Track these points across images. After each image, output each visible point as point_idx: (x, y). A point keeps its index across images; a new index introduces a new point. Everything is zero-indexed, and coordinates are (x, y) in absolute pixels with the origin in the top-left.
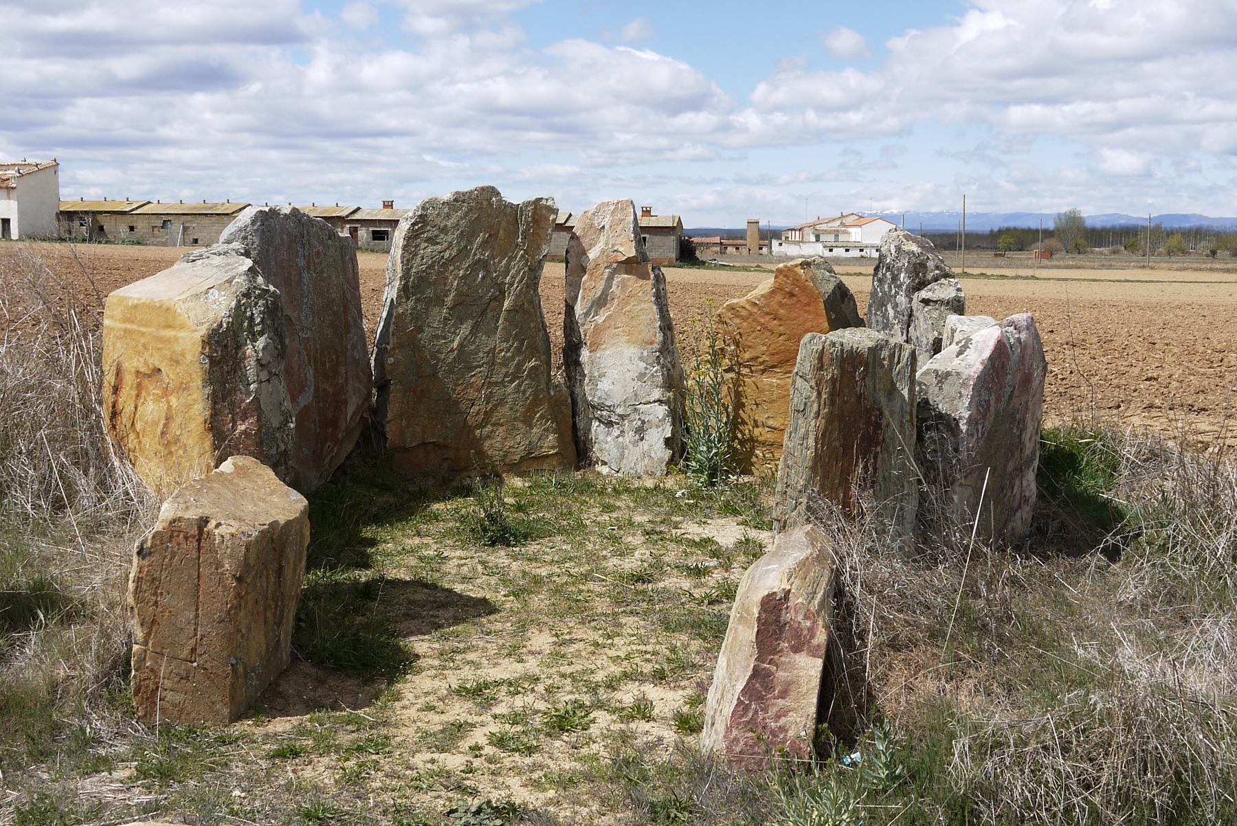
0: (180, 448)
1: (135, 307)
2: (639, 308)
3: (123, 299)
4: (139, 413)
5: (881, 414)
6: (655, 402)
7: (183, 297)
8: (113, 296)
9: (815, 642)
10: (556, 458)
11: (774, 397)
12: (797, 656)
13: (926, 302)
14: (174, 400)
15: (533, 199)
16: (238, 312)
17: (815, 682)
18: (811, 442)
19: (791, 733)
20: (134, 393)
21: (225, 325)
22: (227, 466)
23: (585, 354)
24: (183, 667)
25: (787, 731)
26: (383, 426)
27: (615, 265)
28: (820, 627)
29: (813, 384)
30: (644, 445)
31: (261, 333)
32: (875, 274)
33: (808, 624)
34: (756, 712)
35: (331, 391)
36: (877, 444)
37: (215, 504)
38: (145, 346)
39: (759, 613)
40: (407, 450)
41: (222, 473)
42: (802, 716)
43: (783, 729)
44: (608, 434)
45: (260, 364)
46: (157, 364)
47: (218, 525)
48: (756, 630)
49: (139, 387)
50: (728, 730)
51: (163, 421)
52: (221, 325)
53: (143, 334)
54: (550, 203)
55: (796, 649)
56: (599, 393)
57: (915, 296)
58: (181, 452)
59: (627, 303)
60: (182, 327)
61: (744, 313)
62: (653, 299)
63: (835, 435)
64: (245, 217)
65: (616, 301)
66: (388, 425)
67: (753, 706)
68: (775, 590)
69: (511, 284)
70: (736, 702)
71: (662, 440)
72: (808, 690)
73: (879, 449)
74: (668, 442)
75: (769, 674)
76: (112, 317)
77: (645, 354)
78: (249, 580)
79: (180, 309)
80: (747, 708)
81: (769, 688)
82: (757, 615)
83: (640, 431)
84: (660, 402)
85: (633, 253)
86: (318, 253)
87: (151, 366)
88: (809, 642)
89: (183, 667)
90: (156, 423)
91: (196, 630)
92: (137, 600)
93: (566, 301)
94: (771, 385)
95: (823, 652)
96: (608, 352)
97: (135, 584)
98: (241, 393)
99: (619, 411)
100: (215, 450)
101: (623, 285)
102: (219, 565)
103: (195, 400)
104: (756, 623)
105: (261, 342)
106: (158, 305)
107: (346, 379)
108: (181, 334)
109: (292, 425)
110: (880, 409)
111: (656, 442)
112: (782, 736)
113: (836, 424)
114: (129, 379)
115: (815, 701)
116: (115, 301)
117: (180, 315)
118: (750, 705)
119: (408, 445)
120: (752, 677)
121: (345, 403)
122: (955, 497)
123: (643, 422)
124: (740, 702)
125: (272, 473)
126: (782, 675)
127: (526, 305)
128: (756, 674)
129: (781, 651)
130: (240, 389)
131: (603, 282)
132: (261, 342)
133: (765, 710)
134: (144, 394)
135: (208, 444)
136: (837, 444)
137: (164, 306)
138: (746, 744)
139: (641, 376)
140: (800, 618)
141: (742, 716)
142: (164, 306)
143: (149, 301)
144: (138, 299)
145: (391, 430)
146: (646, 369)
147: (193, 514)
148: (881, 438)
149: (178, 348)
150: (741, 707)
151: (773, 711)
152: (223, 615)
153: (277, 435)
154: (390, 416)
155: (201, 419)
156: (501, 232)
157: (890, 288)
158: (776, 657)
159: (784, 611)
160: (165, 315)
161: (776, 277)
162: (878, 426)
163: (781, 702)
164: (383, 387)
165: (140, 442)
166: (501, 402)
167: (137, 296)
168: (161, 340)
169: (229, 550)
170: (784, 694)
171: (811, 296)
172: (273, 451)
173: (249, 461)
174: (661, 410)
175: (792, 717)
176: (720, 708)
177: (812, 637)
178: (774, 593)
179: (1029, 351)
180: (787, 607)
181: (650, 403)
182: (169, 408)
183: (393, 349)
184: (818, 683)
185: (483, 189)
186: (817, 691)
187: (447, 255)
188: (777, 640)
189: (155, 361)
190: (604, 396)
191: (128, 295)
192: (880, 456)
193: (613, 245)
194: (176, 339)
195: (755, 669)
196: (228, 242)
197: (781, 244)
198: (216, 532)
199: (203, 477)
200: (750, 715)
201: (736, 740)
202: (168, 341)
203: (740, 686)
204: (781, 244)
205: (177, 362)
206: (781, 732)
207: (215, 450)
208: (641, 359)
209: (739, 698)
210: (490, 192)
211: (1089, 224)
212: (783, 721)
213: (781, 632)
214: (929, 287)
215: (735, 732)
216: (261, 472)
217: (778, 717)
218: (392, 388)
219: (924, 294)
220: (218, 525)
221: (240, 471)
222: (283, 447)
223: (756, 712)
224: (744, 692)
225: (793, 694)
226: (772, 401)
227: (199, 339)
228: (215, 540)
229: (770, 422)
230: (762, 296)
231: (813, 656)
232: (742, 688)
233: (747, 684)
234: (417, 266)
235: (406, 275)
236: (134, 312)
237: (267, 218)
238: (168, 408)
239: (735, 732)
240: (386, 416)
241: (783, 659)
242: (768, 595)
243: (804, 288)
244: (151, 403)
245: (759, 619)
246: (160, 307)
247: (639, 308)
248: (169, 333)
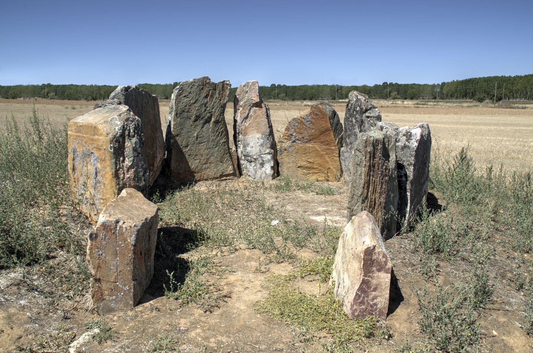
2: (261, 120)
3: (76, 123)
6: (267, 153)
7: (101, 122)
9: (387, 267)
11: (310, 151)
12: (380, 274)
13: (368, 117)
15: (222, 81)
16: (124, 129)
17: (388, 284)
18: (363, 177)
19: (379, 306)
21: (119, 134)
22: (124, 193)
23: (241, 137)
24: (112, 285)
25: (377, 305)
27: (252, 105)
28: (389, 261)
29: (363, 153)
30: (263, 169)
31: (134, 136)
32: (347, 107)
33: (384, 260)
34: (364, 298)
35: (151, 153)
37: (121, 213)
39: (364, 256)
41: (122, 197)
42: (383, 299)
43: (375, 304)
44: (251, 165)
45: (135, 150)
47: (124, 223)
48: (362, 263)
50: (352, 306)
52: (117, 134)
53: (84, 137)
54: (228, 82)
55: (379, 270)
57: (364, 115)
59: (256, 118)
60: (101, 135)
61: (299, 121)
62: (266, 117)
64: (119, 89)
65: (252, 118)
67: (363, 295)
68: (370, 246)
69: (215, 112)
71: (270, 167)
72: (385, 287)
74: (272, 168)
75: (369, 281)
76: (71, 131)
79: (100, 127)
80: (360, 296)
81: (369, 287)
82: (363, 257)
83: (262, 165)
84: (269, 153)
85: (258, 100)
86: (145, 103)
88: (385, 267)
89: (112, 285)
91: (117, 268)
92: (91, 258)
93: (463, 148)
94: (309, 147)
95: (390, 271)
96: (250, 136)
97: (90, 251)
99: (255, 157)
100: (117, 185)
101: (255, 112)
102: (125, 240)
103: (107, 165)
104: (362, 260)
105: (134, 140)
106: (90, 125)
107: (157, 149)
108: (101, 138)
111: (268, 169)
112: (375, 307)
115: (388, 292)
116: (72, 124)
117: (100, 130)
120: (361, 283)
121: (156, 157)
124: (357, 294)
125: (142, 195)
126: (374, 282)
128: (364, 282)
129: (373, 271)
131: (248, 111)
132: (134, 140)
133: (368, 297)
135: (114, 184)
137: (93, 126)
138: (360, 312)
139: (262, 145)
140: (381, 257)
141: (357, 300)
142: (93, 126)
143: (86, 124)
144: (82, 123)
147: (113, 219)
149: (100, 144)
150: (357, 296)
151: (371, 297)
152: (128, 261)
155: (110, 173)
158: (371, 274)
159: (373, 255)
160: (93, 129)
161: (311, 108)
163: (374, 293)
166: (212, 155)
167: (81, 122)
168: (92, 140)
169: (129, 234)
170: (375, 290)
171: (324, 114)
173: (132, 190)
174: (269, 157)
175: (379, 299)
176: (347, 296)
177: (386, 265)
178: (370, 247)
180: (375, 253)
181: (265, 154)
184: (389, 285)
185: (204, 78)
186: (389, 288)
187: (191, 102)
188: (371, 267)
190: (249, 152)
191: (78, 121)
193: (251, 97)
194: (99, 140)
195: (363, 280)
196: (113, 99)
198: (124, 226)
199: (115, 199)
200: (361, 299)
201: (356, 310)
202: (96, 140)
203: (357, 287)
205: (100, 149)
206: (375, 306)
207: (117, 185)
208: (262, 138)
209: (356, 293)
211: (88, 86)
212: (375, 301)
213: (373, 264)
214: (368, 112)
215: (355, 307)
216: (138, 195)
217: (373, 299)
218: (173, 151)
219: (367, 114)
220: (124, 223)
221: (130, 195)
223: (364, 298)
224: (358, 290)
225: (379, 290)
226: (310, 153)
227: (109, 140)
228: (123, 229)
229: (309, 160)
231: (387, 273)
232: (357, 288)
233: (360, 286)
234: (181, 106)
235: (177, 108)
236: (80, 128)
237: (127, 89)
239: (355, 307)
241: (374, 275)
242: (368, 248)
243: (321, 112)
245: (364, 259)
246: (91, 127)
247: (261, 120)
248: (96, 137)
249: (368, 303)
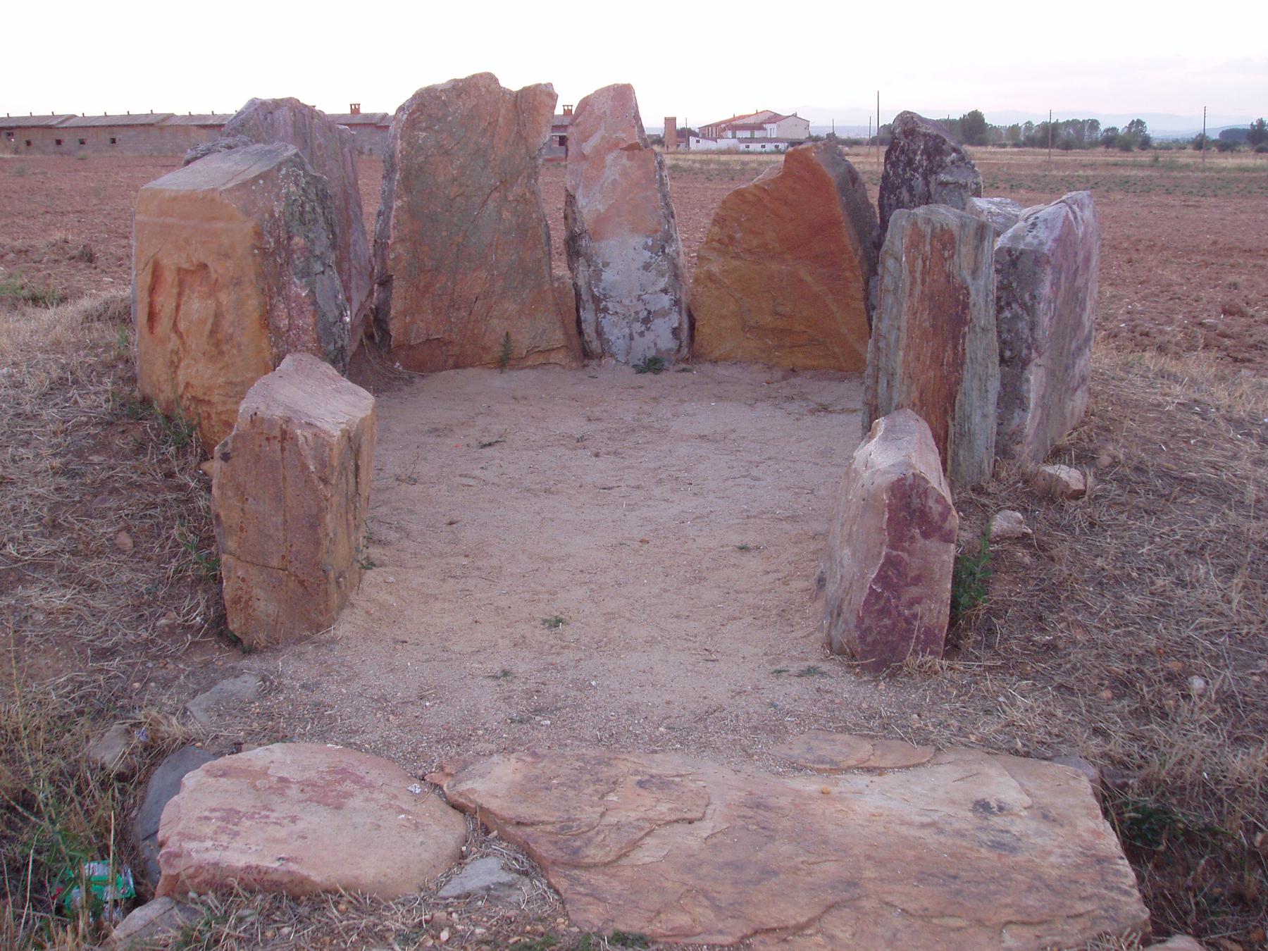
0: (233, 347)
1: (174, 199)
4: (181, 313)
5: (968, 293)
7: (229, 185)
8: (146, 190)
10: (562, 351)
14: (223, 297)
20: (175, 291)
26: (386, 323)
36: (965, 324)
38: (187, 241)
39: (890, 499)
40: (411, 347)
46: (203, 259)
49: (181, 284)
50: (860, 620)
51: (210, 321)
56: (602, 285)
58: (235, 351)
63: (926, 316)
66: (391, 322)
67: (886, 594)
70: (868, 591)
73: (967, 329)
77: (650, 243)
78: (333, 482)
87: (195, 262)
90: (204, 322)
98: (296, 286)
103: (249, 296)
106: (201, 196)
109: (348, 319)
110: (967, 288)
113: (927, 303)
114: (169, 277)
118: (882, 592)
119: (412, 343)
122: (1032, 378)
123: (649, 312)
127: (528, 195)
130: (294, 283)
134: (187, 291)
136: (927, 324)
139: (647, 267)
144: (177, 191)
145: (395, 327)
146: (651, 258)
148: (968, 318)
151: (905, 598)
153: (334, 330)
154: (393, 312)
156: (501, 119)
157: (904, 170)
162: (966, 306)
164: (385, 282)
165: (184, 344)
172: (331, 347)
179: (1090, 229)
182: (219, 304)
183: (394, 243)
189: (200, 256)
192: (968, 337)
197: (698, 142)
201: (869, 629)
204: (698, 142)
208: (646, 247)
209: (871, 587)
210: (490, 79)
212: (918, 609)
217: (911, 604)
218: (395, 283)
222: (340, 343)
224: (875, 581)
230: (772, 181)
238: (217, 306)
240: (388, 312)
244: (196, 301)
249: (899, 614)
